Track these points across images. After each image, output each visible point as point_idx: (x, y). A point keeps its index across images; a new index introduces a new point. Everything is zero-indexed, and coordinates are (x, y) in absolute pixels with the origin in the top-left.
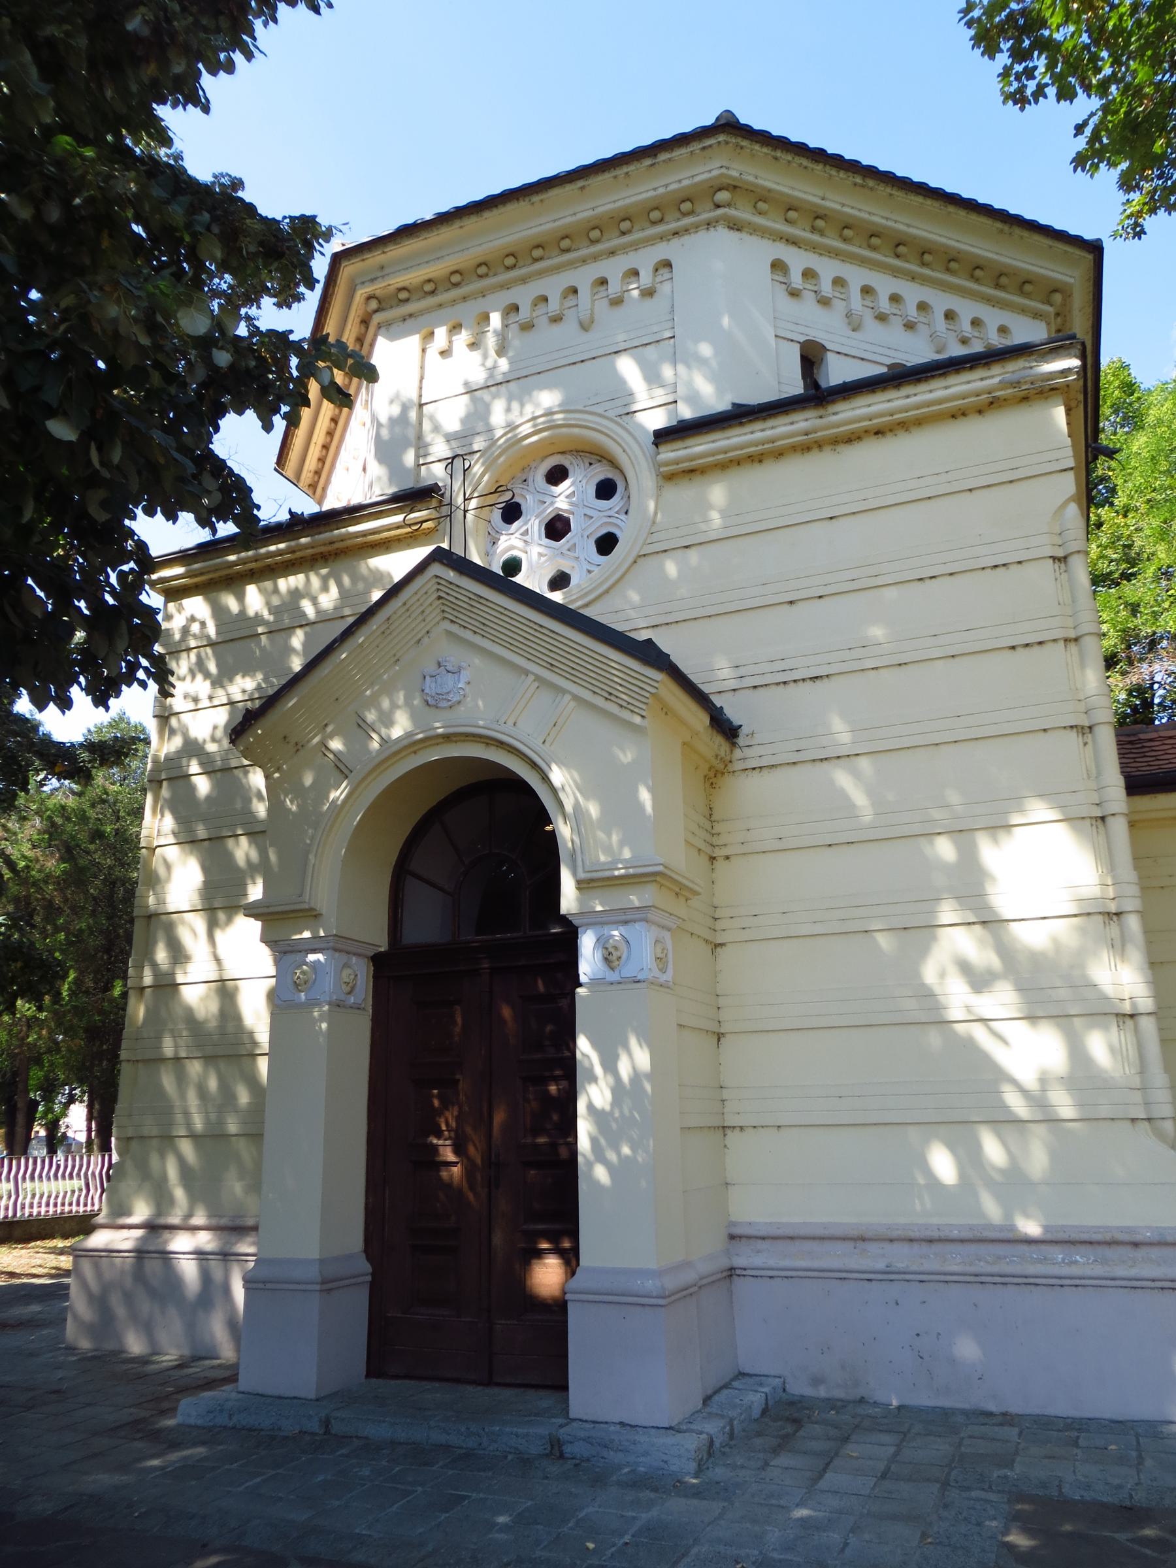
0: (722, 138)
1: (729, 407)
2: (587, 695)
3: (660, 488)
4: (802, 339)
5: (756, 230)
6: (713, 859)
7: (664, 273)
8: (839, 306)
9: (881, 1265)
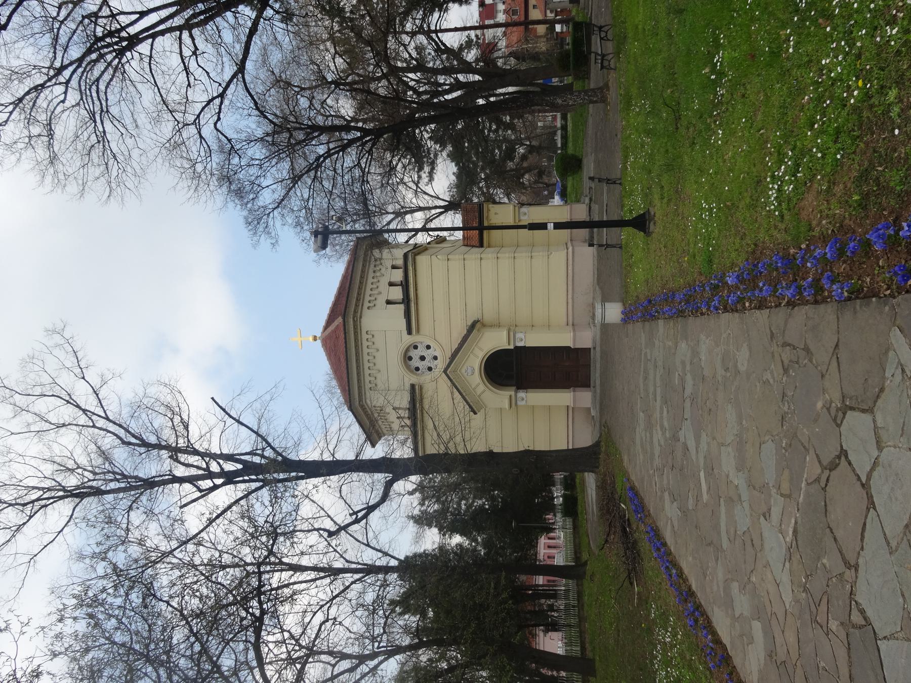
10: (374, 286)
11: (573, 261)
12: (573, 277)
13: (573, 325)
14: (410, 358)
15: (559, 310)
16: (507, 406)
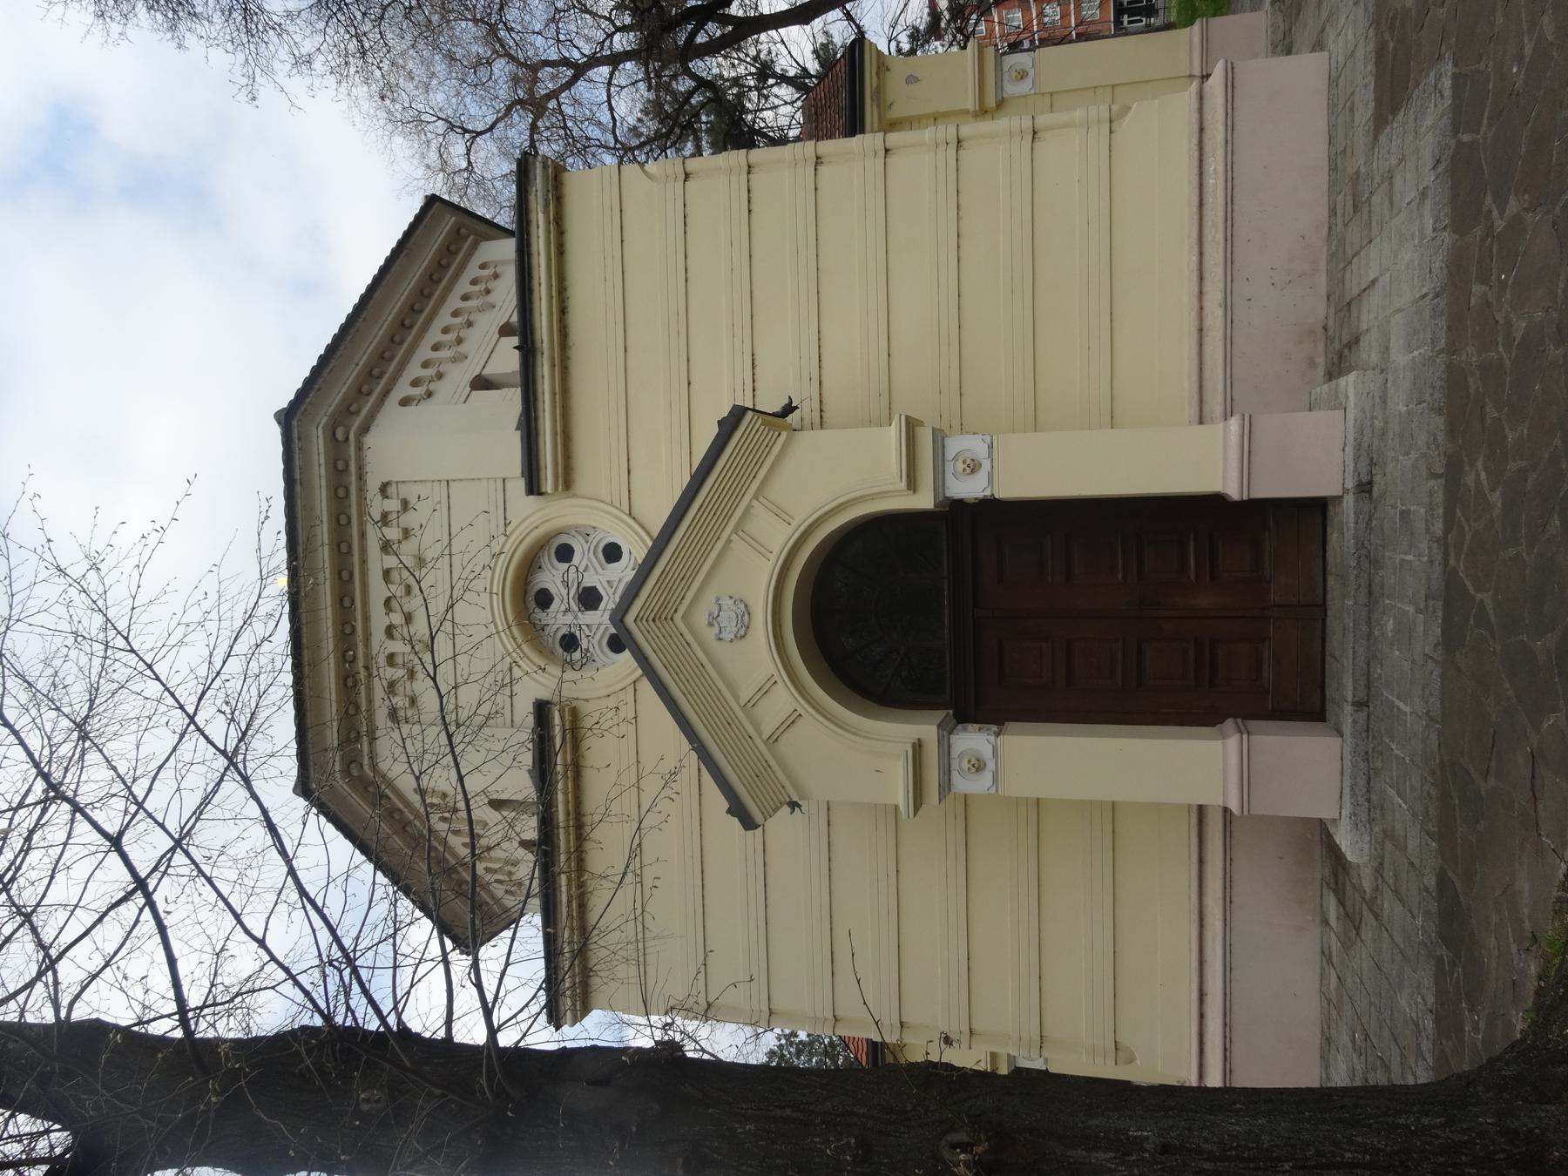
0: (295, 423)
3: (575, 496)
5: (371, 417)
7: (392, 490)
9: (1220, 312)
11: (1230, 127)
14: (544, 599)
16: (899, 794)
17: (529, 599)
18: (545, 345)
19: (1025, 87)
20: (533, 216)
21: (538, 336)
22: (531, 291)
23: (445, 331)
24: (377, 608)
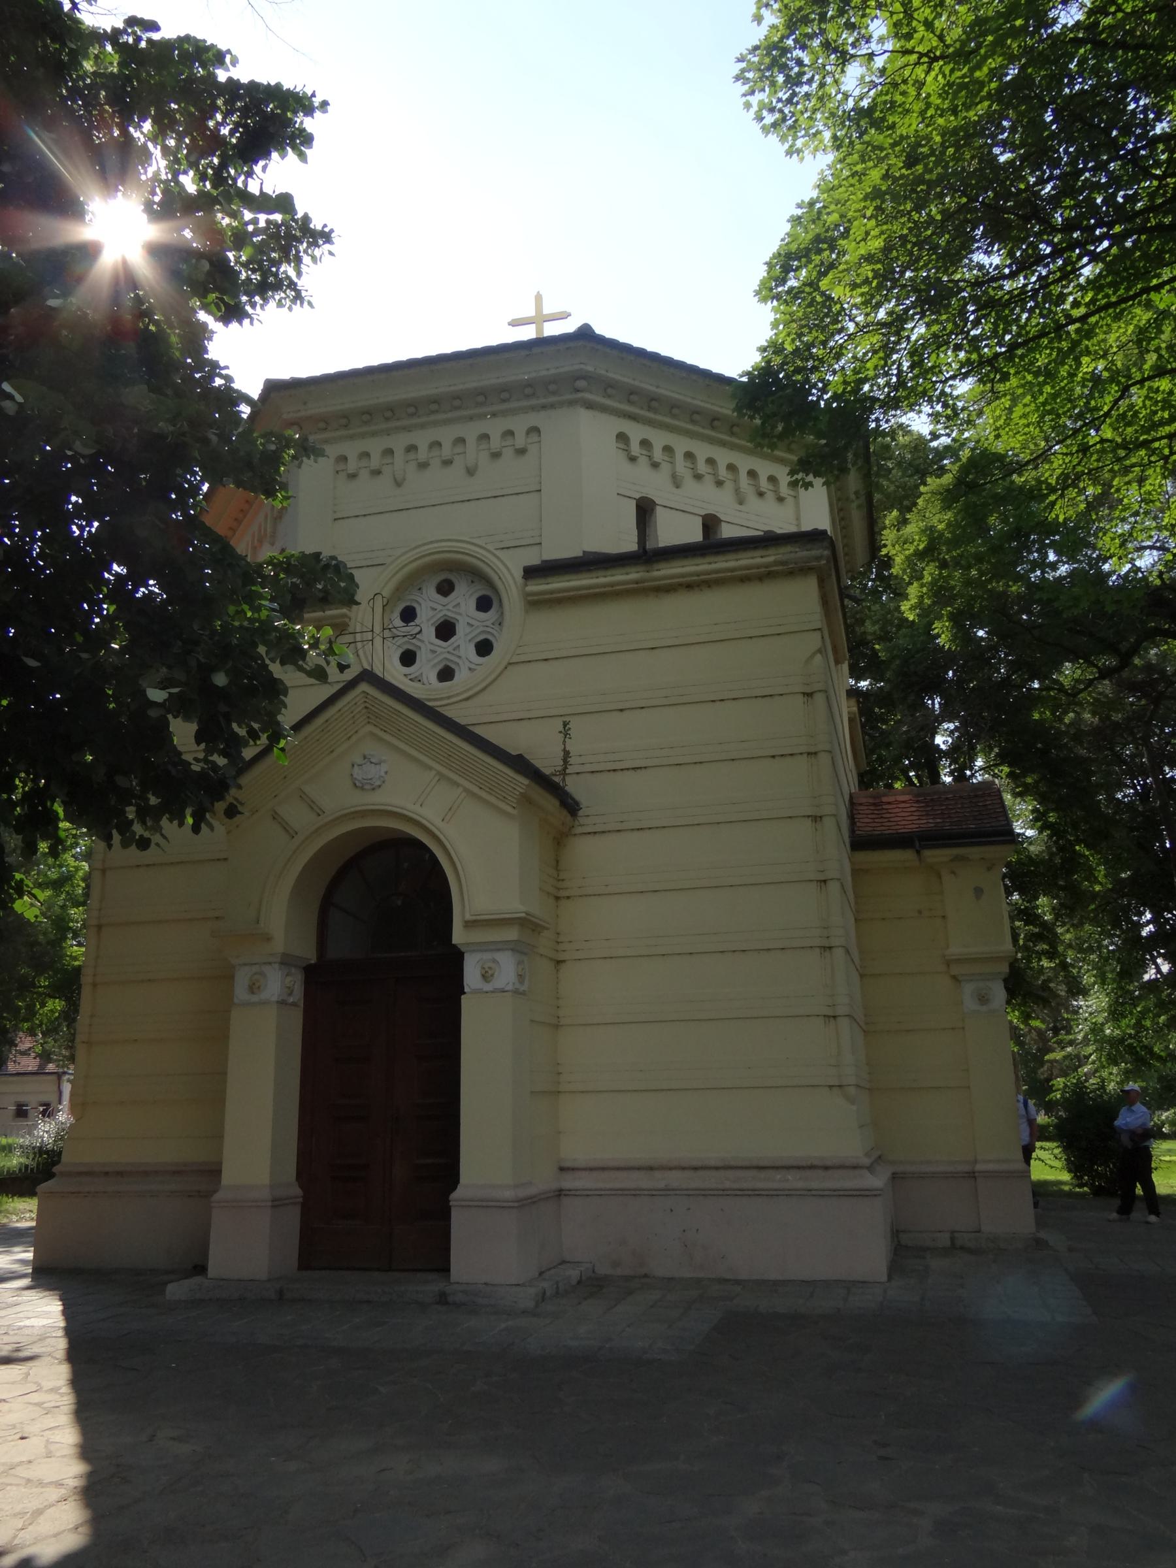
1: (581, 554)
2: (476, 790)
4: (637, 497)
5: (604, 409)
6: (557, 898)
8: (665, 468)
9: (662, 1185)
10: (702, 467)
12: (755, 1193)
13: (560, 1193)
14: (446, 588)
15: (597, 1133)
17: (449, 574)
18: (656, 574)
19: (970, 1004)
20: (772, 551)
21: (662, 565)
22: (703, 555)
23: (711, 462)
24: (431, 434)
